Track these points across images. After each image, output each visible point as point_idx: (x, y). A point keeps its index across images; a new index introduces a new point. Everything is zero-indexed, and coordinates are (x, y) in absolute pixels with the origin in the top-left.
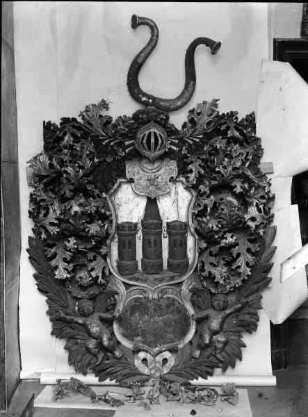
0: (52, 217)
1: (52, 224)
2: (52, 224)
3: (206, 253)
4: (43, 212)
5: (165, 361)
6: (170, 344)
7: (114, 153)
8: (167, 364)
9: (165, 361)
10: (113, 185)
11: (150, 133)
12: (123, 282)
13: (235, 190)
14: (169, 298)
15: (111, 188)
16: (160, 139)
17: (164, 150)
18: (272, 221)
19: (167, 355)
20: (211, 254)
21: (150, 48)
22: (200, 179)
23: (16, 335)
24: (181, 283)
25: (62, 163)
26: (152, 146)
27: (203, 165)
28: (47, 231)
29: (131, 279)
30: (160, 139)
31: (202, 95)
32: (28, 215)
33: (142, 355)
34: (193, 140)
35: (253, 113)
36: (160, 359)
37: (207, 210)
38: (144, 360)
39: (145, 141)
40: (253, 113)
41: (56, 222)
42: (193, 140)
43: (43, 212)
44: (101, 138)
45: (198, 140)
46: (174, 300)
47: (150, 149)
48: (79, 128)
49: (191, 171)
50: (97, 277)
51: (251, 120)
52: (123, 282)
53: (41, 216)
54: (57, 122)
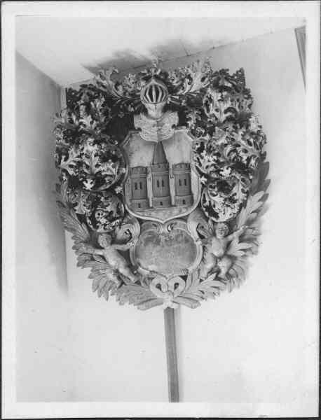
0: (70, 161)
1: (71, 166)
2: (71, 166)
4: (63, 157)
7: (125, 110)
9: (176, 285)
10: (125, 136)
11: (151, 87)
13: (204, 183)
14: (178, 230)
15: (123, 140)
16: (160, 90)
17: (164, 103)
18: (265, 158)
21: (172, 324)
25: (78, 118)
26: (154, 88)
28: (67, 174)
30: (160, 90)
31: (157, 314)
35: (241, 70)
40: (241, 70)
41: (74, 164)
43: (63, 157)
46: (182, 232)
48: (94, 89)
49: (190, 119)
50: (112, 212)
51: (241, 75)
52: (137, 218)
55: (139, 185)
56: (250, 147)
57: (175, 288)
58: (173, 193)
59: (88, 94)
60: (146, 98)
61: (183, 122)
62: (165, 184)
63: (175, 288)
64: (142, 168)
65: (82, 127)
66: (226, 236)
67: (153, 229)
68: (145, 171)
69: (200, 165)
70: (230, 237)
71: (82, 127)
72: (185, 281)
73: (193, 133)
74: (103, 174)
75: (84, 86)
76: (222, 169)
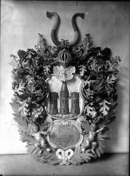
2: (20, 91)
3: (88, 106)
5: (69, 153)
6: (80, 97)
8: (70, 155)
9: (69, 153)
12: (52, 118)
19: (70, 150)
20: (90, 106)
22: (85, 74)
23: (18, 157)
24: (77, 118)
27: (86, 68)
29: (55, 117)
32: (12, 88)
33: (59, 150)
34: (82, 59)
36: (67, 152)
37: (88, 86)
38: (60, 153)
39: (61, 57)
42: (82, 59)
43: (16, 86)
44: (43, 57)
45: (84, 59)
47: (64, 60)
52: (52, 118)
53: (16, 88)
54: (26, 50)
55: (64, 101)
56: (111, 88)
57: (69, 155)
58: (70, 107)
59: (31, 54)
60: (61, 58)
61: (78, 72)
62: (67, 102)
63: (69, 155)
64: (75, 93)
65: (27, 71)
66: (96, 130)
67: (118, 72)
68: (77, 95)
69: (85, 94)
70: (98, 131)
71: (27, 71)
72: (74, 151)
73: (83, 78)
74: (36, 95)
75: (29, 50)
76: (97, 97)
